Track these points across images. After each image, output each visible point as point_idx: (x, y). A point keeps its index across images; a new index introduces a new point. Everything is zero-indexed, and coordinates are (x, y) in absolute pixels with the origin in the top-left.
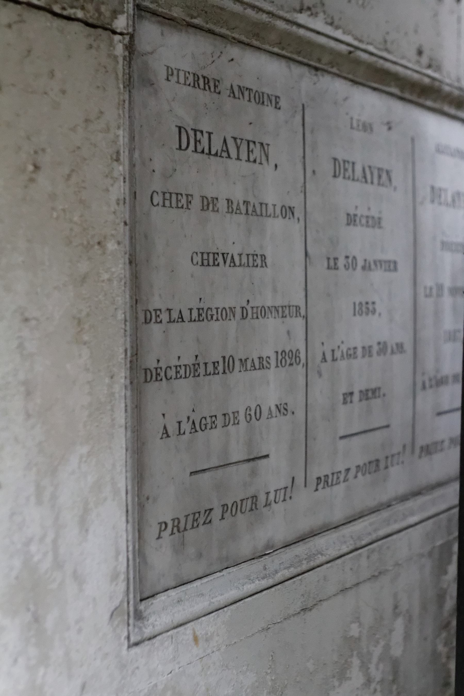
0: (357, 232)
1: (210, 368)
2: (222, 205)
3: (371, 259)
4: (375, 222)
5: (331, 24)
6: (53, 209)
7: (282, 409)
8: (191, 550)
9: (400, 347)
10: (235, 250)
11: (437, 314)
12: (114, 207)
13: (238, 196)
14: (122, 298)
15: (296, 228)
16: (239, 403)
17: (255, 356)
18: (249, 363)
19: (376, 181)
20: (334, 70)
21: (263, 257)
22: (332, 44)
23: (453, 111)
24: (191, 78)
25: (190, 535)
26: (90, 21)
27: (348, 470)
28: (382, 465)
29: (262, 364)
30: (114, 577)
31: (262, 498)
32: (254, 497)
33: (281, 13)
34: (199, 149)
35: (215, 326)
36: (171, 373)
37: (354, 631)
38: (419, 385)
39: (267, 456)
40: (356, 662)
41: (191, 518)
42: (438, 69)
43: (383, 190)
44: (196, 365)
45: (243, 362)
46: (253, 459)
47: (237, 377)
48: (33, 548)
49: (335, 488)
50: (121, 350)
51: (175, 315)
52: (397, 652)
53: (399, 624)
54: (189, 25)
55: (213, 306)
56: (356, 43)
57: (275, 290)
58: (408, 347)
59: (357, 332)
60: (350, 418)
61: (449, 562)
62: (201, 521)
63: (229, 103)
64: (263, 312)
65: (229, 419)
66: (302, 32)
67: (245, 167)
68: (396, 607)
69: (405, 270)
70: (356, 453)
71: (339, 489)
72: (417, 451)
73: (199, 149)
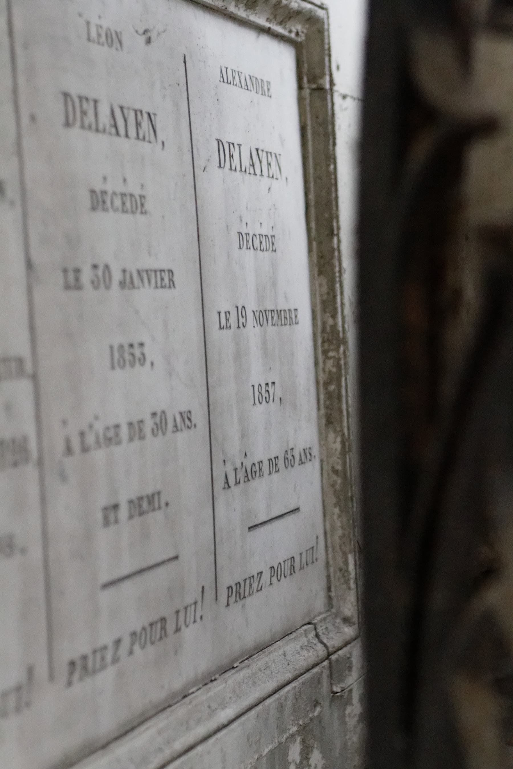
4: (135, 204)
9: (187, 417)
11: (239, 356)
19: (132, 132)
23: (242, 13)
28: (170, 627)
38: (220, 483)
58: (199, 418)
60: (115, 549)
70: (129, 610)
71: (107, 678)
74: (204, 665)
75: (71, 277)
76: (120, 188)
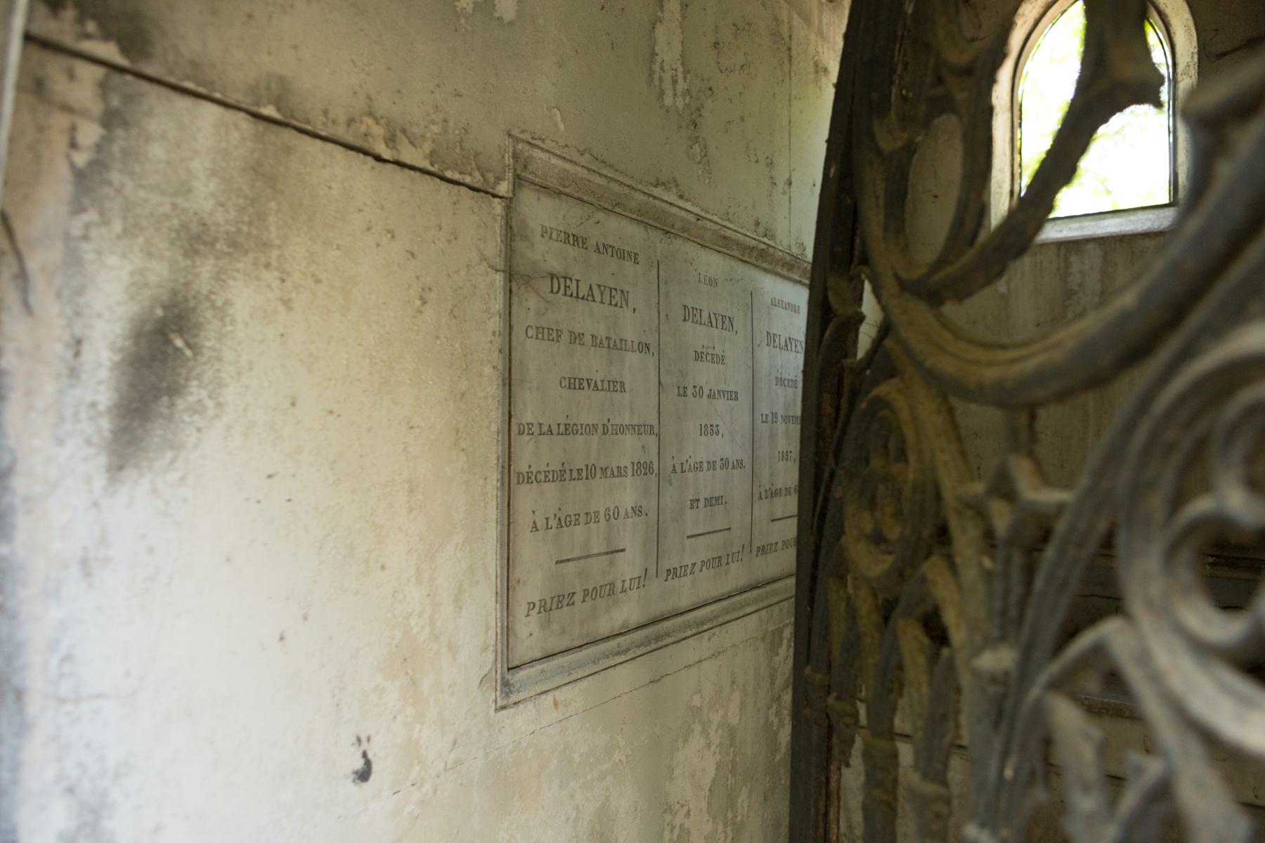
0: (702, 366)
1: (575, 474)
2: (588, 339)
3: (715, 388)
4: (721, 360)
5: (681, 197)
6: (437, 337)
7: (637, 511)
8: (556, 627)
9: (740, 463)
10: (598, 377)
11: (773, 436)
12: (490, 338)
13: (601, 332)
14: (496, 414)
15: (651, 362)
16: (600, 504)
17: (614, 466)
18: (609, 472)
19: (720, 325)
20: (685, 235)
21: (622, 384)
22: (683, 213)
23: (785, 273)
24: (562, 235)
25: (555, 613)
26: (476, 186)
27: (694, 564)
28: (724, 561)
29: (620, 472)
30: (484, 649)
31: (619, 585)
32: (612, 584)
33: (639, 187)
34: (569, 293)
35: (580, 439)
36: (541, 477)
37: (696, 701)
38: (756, 496)
39: (623, 550)
40: (697, 728)
41: (556, 600)
42: (773, 237)
43: (726, 333)
44: (563, 471)
45: (604, 470)
46: (612, 552)
47: (598, 482)
48: (413, 622)
49: (683, 579)
50: (494, 457)
51: (545, 429)
52: (734, 720)
53: (737, 696)
54: (561, 193)
55: (578, 423)
56: (702, 214)
57: (632, 411)
58: (747, 463)
59: (700, 449)
60: (694, 520)
61: (781, 645)
62: (565, 602)
63: (595, 257)
64: (621, 429)
65: (591, 517)
66: (657, 202)
67: (608, 310)
68: (733, 682)
69: (744, 398)
70: (701, 550)
71: (687, 581)
72: (755, 550)
73: (569, 293)
74: (742, 582)
75: (682, 390)
76: (711, 351)
